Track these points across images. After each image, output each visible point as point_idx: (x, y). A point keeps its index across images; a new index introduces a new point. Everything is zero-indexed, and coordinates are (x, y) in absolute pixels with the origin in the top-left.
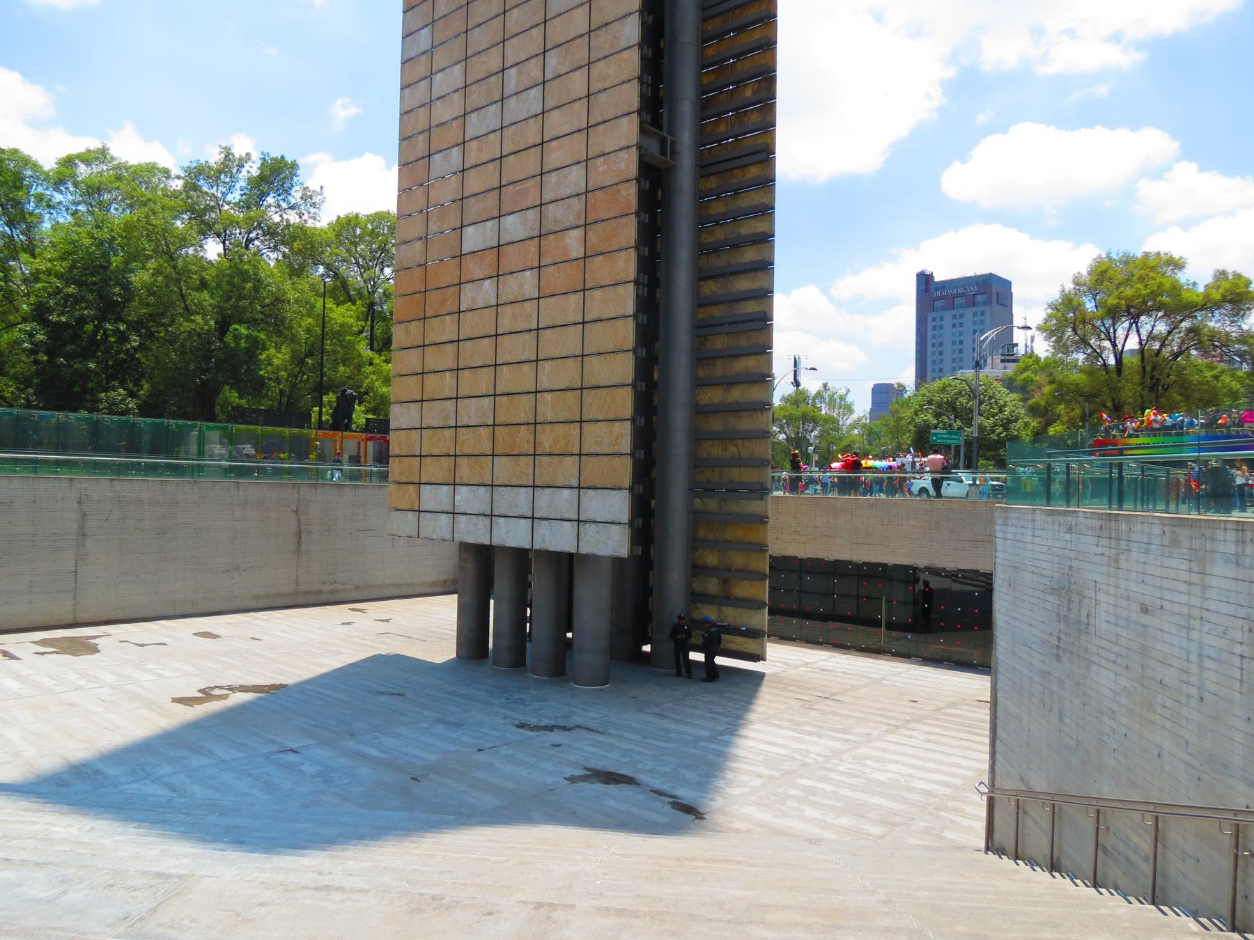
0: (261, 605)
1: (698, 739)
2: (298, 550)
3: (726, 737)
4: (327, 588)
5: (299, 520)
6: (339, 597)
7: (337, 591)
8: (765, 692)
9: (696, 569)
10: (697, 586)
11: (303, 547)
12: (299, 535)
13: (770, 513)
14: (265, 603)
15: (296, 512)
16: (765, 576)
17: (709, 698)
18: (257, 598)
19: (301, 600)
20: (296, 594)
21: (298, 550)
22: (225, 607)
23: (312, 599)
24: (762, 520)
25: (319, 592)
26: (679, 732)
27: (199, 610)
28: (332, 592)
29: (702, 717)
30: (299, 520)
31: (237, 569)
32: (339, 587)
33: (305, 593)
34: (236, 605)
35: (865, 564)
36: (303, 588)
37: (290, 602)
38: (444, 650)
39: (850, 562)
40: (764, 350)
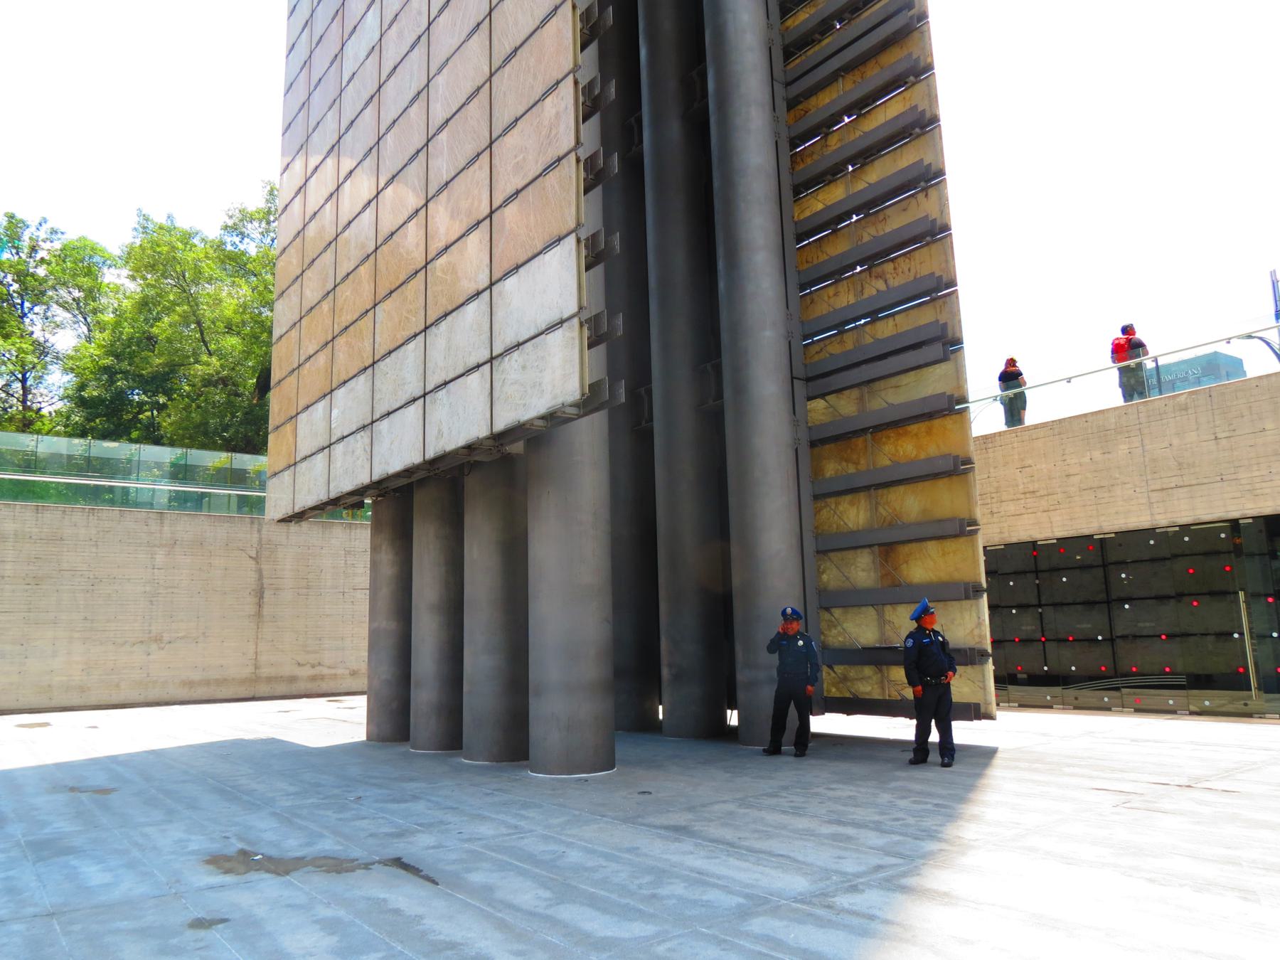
0: (195, 696)
1: (759, 903)
2: (259, 614)
3: (868, 899)
4: (306, 672)
5: (260, 572)
6: (325, 686)
7: (322, 677)
8: (997, 773)
9: (821, 545)
10: (831, 577)
11: (266, 611)
12: (260, 594)
13: (979, 513)
14: (200, 692)
15: (256, 559)
16: (983, 654)
17: (845, 791)
18: (190, 684)
19: (263, 689)
20: (255, 679)
21: (259, 614)
22: (134, 696)
23: (282, 688)
24: (956, 468)
25: (293, 679)
26: (701, 879)
27: (93, 700)
28: (313, 678)
29: (809, 834)
30: (260, 572)
31: (158, 639)
32: (325, 671)
33: (269, 680)
34: (153, 694)
35: (1185, 528)
36: (265, 671)
37: (243, 692)
38: (358, 733)
39: (1150, 532)
40: (944, 344)
